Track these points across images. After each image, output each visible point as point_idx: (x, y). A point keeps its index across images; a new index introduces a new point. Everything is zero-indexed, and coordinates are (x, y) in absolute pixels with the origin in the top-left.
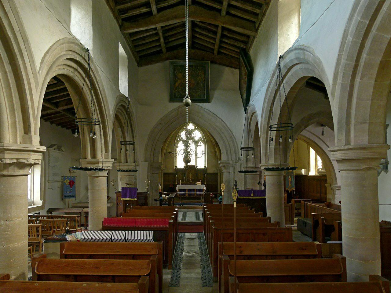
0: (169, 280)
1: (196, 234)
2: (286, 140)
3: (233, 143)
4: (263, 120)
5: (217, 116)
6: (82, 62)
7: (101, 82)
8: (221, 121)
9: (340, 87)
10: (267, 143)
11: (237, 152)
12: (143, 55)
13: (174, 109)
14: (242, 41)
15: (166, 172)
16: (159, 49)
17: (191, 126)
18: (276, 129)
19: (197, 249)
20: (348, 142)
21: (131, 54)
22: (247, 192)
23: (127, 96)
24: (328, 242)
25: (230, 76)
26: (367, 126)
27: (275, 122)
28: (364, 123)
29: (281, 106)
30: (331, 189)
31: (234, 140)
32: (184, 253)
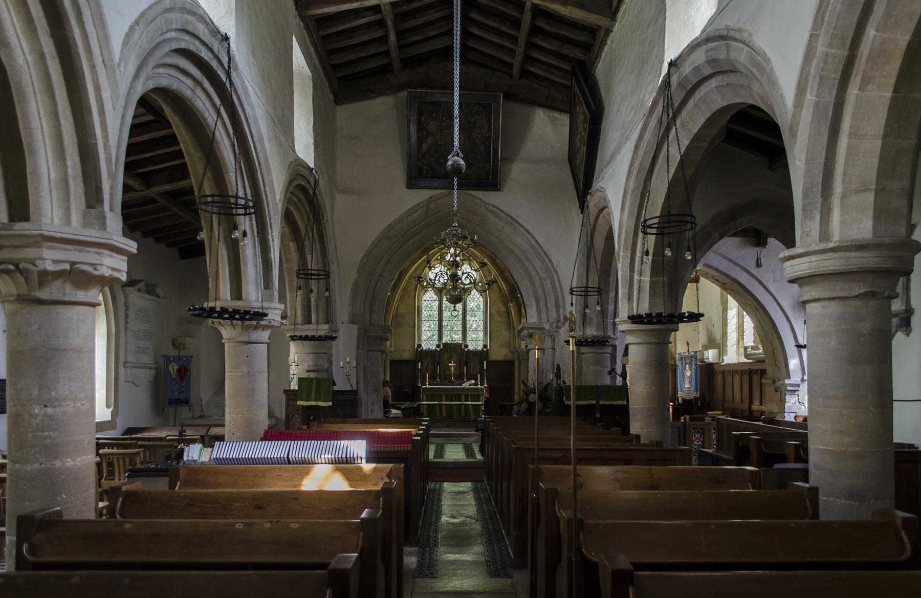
0: (414, 566)
1: (469, 484)
2: (678, 256)
3: (553, 283)
4: (625, 218)
5: (516, 221)
6: (214, 64)
7: (256, 122)
8: (525, 233)
9: (811, 110)
10: (632, 270)
11: (561, 304)
12: (347, 72)
13: (419, 204)
15: (396, 357)
16: (385, 62)
18: (654, 231)
20: (825, 235)
21: (321, 71)
23: (312, 166)
24: (776, 466)
25: (547, 131)
26: (870, 198)
28: (864, 191)
29: (670, 178)
30: (776, 390)
31: (555, 276)
32: (444, 518)
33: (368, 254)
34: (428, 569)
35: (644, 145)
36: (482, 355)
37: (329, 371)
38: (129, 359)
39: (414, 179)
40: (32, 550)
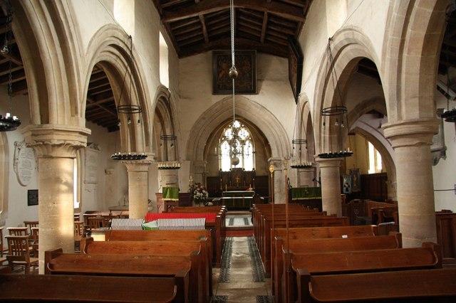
3: (284, 138)
6: (125, 48)
12: (183, 47)
14: (289, 28)
15: (209, 176)
17: (237, 124)
19: (247, 250)
20: (400, 117)
22: (299, 191)
23: (167, 87)
25: (277, 66)
27: (328, 104)
32: (233, 255)
33: (195, 127)
34: (224, 278)
35: (321, 74)
36: (252, 174)
37: (176, 184)
38: (87, 179)
39: (216, 91)
40: (51, 266)
